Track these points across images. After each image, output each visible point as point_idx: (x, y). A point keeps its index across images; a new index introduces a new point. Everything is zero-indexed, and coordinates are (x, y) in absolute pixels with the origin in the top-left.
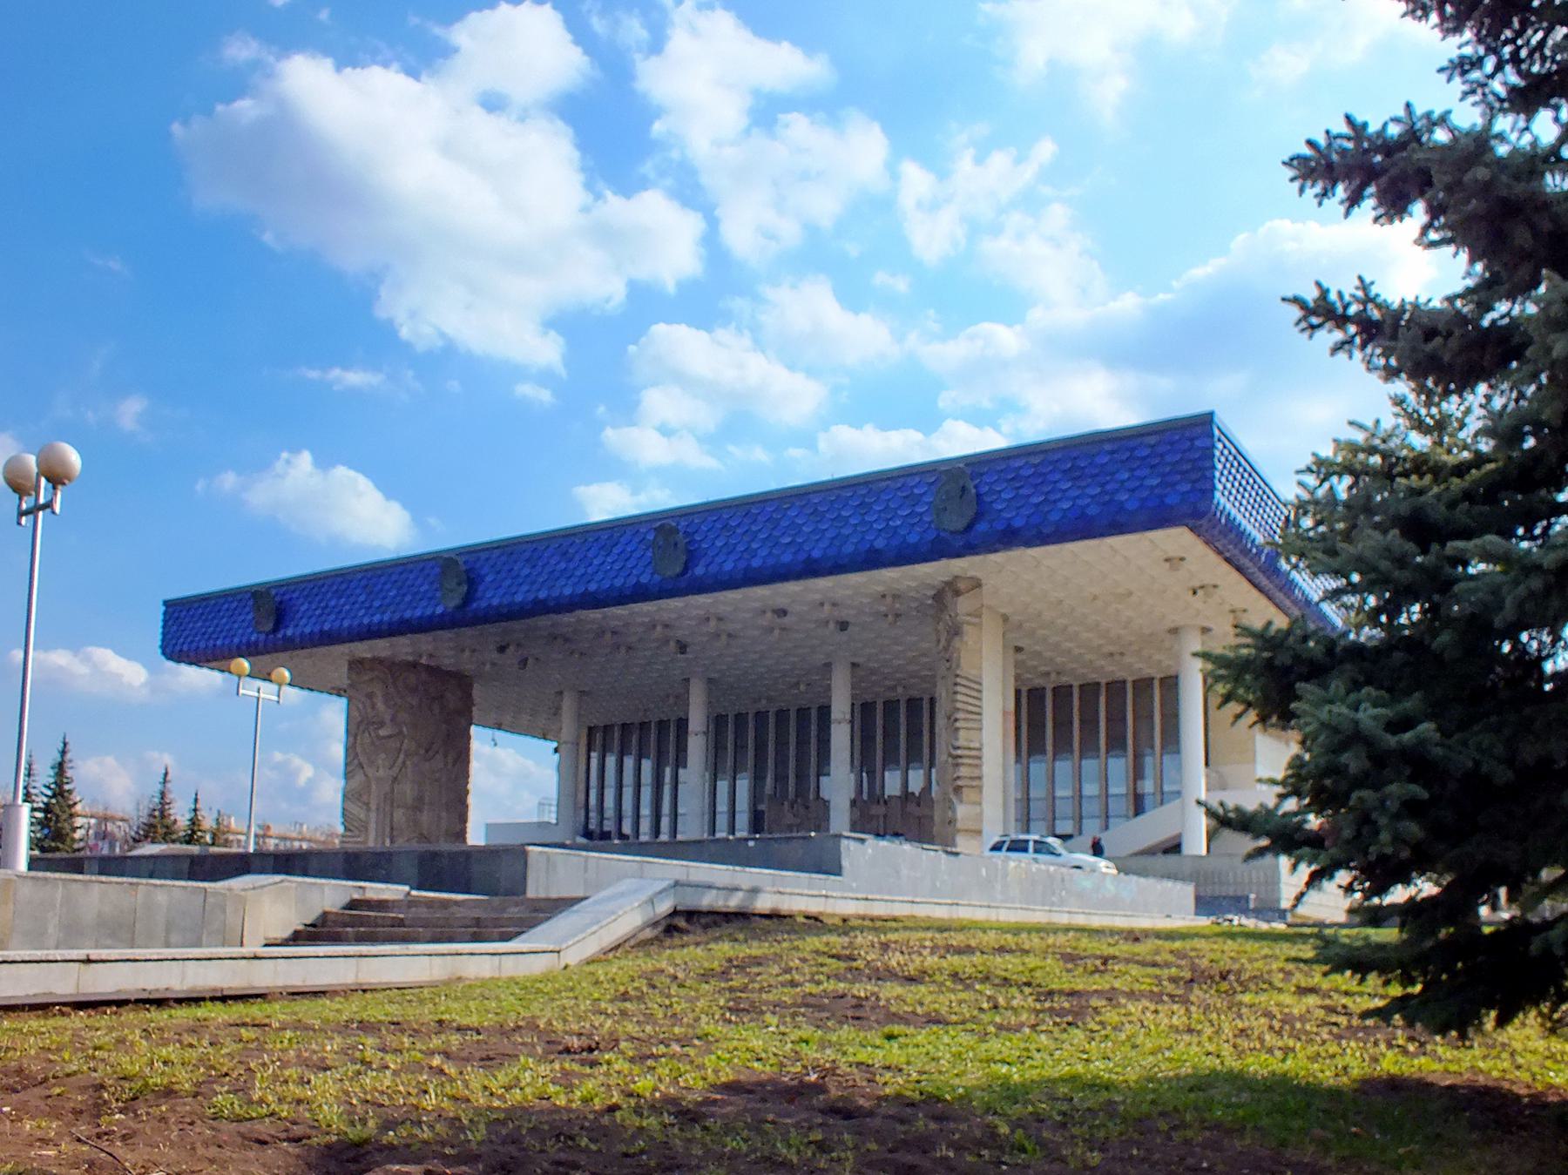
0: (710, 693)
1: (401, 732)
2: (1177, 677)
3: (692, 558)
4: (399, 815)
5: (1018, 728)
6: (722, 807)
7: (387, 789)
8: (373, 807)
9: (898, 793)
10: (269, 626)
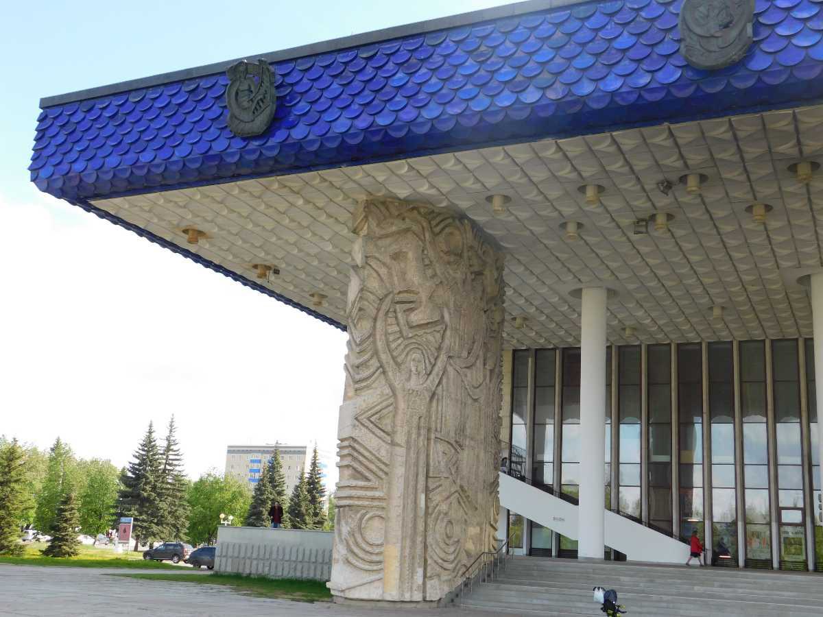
3: (280, 117)
4: (438, 451)
5: (608, 385)
6: (362, 450)
7: (423, 410)
8: (400, 438)
10: (260, 122)
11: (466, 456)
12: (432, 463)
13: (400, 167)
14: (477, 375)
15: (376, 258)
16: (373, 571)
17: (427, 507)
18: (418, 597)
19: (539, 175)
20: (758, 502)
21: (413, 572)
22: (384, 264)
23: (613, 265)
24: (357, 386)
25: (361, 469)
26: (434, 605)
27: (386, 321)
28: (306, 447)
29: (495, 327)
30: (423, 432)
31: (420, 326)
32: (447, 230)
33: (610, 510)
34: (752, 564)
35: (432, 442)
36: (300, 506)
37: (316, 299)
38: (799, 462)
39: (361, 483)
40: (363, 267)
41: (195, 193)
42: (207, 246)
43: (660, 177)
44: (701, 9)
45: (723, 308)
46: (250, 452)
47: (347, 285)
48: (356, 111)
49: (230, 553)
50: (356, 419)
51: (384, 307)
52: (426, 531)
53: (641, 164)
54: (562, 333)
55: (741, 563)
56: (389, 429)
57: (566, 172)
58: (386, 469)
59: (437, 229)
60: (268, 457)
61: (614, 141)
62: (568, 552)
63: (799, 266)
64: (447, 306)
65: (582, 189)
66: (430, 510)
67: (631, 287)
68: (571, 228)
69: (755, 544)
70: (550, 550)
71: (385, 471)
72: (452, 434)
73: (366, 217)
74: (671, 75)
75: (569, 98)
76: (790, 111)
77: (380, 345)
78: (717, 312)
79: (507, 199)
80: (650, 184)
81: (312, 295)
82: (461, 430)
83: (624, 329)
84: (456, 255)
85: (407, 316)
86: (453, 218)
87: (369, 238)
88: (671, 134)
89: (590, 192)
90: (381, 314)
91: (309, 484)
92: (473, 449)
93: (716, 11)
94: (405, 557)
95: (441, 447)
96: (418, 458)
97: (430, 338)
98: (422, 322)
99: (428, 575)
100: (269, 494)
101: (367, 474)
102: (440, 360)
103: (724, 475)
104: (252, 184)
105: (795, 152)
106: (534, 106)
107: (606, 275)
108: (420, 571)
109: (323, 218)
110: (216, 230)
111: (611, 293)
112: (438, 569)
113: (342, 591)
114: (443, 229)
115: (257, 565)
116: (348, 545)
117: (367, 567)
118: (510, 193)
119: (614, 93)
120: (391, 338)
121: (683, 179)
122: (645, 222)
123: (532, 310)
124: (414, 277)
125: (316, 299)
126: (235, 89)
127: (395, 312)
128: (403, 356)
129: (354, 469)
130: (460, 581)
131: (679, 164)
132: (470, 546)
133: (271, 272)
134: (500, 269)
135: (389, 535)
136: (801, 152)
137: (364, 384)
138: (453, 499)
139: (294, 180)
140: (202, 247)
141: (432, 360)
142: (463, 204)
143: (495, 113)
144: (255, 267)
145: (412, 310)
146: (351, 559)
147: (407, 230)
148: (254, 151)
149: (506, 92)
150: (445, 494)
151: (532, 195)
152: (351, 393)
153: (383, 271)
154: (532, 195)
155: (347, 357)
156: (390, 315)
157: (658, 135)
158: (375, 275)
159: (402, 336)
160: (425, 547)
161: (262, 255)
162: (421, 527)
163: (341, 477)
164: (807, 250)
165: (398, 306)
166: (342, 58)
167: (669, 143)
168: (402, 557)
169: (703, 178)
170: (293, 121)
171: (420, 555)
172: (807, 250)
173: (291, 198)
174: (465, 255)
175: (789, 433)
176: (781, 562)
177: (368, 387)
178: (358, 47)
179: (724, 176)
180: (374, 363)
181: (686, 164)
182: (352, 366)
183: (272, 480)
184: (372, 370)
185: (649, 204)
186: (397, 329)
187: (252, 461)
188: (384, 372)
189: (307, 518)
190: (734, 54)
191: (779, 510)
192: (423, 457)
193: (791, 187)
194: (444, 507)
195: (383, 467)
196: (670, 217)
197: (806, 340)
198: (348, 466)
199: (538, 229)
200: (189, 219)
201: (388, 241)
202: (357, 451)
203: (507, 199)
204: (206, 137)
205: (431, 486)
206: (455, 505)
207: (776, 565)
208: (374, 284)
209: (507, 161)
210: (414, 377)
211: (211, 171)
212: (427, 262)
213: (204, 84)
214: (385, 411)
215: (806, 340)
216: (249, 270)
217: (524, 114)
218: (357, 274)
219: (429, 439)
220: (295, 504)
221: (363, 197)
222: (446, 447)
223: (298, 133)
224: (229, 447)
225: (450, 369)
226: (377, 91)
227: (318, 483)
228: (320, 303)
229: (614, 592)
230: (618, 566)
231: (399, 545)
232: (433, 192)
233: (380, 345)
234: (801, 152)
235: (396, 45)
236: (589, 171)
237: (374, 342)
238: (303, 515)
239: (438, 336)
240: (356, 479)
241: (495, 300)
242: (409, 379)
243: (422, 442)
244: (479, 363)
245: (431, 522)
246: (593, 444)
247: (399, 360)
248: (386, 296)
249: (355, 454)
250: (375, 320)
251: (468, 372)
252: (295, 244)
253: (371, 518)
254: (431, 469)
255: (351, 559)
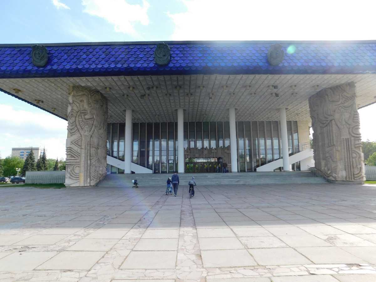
0: (184, 114)
1: (93, 118)
2: (229, 122)
3: (49, 62)
4: (93, 151)
6: (73, 150)
8: (83, 147)
9: (194, 147)
10: (43, 63)
11: (99, 151)
12: (91, 153)
13: (84, 79)
14: (101, 131)
15: (76, 101)
16: (77, 180)
17: (90, 164)
18: (88, 185)
19: (119, 83)
20: (164, 159)
21: (87, 179)
22: (78, 103)
23: (134, 105)
24: (71, 134)
25: (73, 155)
26: (92, 187)
27: (79, 118)
28: (38, 148)
29: (106, 119)
30: (89, 145)
31: (88, 119)
32: (95, 95)
33: (133, 162)
34: (163, 172)
35: (91, 147)
36: (40, 164)
37: (53, 109)
38: (173, 150)
39: (73, 158)
40: (72, 104)
41: (20, 80)
42: (21, 94)
43: (148, 86)
44: (159, 51)
45: (158, 115)
46: (20, 150)
47: (67, 109)
48: (71, 63)
49: (30, 178)
50: (71, 142)
51: (78, 114)
52: (90, 169)
53: (143, 83)
54: (120, 120)
55: (160, 172)
56: (80, 145)
57: (126, 84)
58: (80, 155)
59: (92, 94)
60: (30, 151)
61: (138, 78)
62: (122, 172)
63: (175, 107)
64: (94, 114)
65: (129, 88)
66: (91, 164)
67: (138, 110)
68: (126, 96)
69: (163, 168)
70: (116, 172)
71: (79, 155)
72: (96, 146)
73: (73, 90)
74: (152, 65)
75: (128, 67)
76: (176, 76)
77: (77, 124)
78: (157, 116)
79: (110, 88)
80: (145, 87)
81: (52, 108)
82: (98, 145)
83: (135, 119)
84: (97, 101)
85: (84, 116)
86: (96, 92)
87: (74, 96)
88: (151, 78)
89: (131, 89)
90: (77, 116)
91: (42, 158)
92: (101, 149)
93: (162, 52)
94: (324, 159)
95: (94, 149)
96: (88, 152)
97: (90, 122)
98: (88, 118)
99: (91, 179)
100: (30, 161)
101: (74, 156)
102: (93, 128)
103: (157, 153)
104: (39, 79)
105: (177, 84)
106: (120, 68)
107: (132, 107)
108: (89, 179)
109: (59, 89)
110: (25, 90)
111: (133, 111)
112: (94, 178)
113: (69, 185)
114: (94, 94)
115: (39, 181)
116: (70, 174)
117: (75, 179)
118: (111, 87)
119: (139, 67)
120: (80, 122)
121: (153, 87)
122: (143, 96)
123: (113, 114)
124: (86, 106)
125: (53, 109)
126: (34, 53)
127: (81, 115)
128: (84, 126)
129: (71, 155)
130: (98, 180)
131: (152, 84)
132: (100, 172)
133: (41, 102)
134: (107, 105)
135: (81, 171)
136: (178, 84)
137: (73, 134)
138: (97, 161)
139: (52, 79)
140: (20, 94)
141: (91, 127)
142: (99, 89)
143: (110, 69)
144: (36, 100)
145: (85, 115)
146: (71, 177)
147: (84, 94)
148: (41, 71)
149: (113, 64)
150: (95, 160)
151: (117, 88)
152: (70, 136)
153: (78, 105)
154: (117, 88)
155: (68, 127)
156: (80, 116)
157: (148, 78)
158: (76, 106)
159: (83, 121)
160: (90, 173)
161: (17, 86)
162: (89, 168)
163: (67, 157)
164: (177, 101)
165: (82, 114)
166: (67, 48)
167: (150, 80)
168: (84, 175)
169: (157, 87)
170: (53, 64)
171: (88, 175)
172: (177, 101)
173: (50, 84)
174: (99, 101)
175: (171, 143)
176: (161, 172)
177: (74, 134)
178: (72, 46)
179: (162, 87)
180: (76, 128)
181: (154, 84)
182: (70, 129)
183: (31, 158)
184: (75, 130)
185: (144, 92)
186: (82, 120)
187: (21, 152)
188: (78, 131)
189: (42, 168)
190: (166, 62)
191: (169, 160)
192: (89, 152)
193: (176, 91)
194: (94, 163)
195: (79, 154)
196: (149, 95)
197: (175, 123)
198: (69, 154)
199: (117, 96)
200: (16, 86)
201: (79, 97)
202: (72, 151)
203: (110, 88)
204: (25, 65)
205: (91, 158)
206: (97, 163)
207: (167, 172)
208: (75, 108)
209: (112, 80)
210: (86, 132)
211: (25, 74)
212: (89, 103)
213: (23, 49)
214: (79, 141)
215: (175, 123)
216: (33, 101)
217: (117, 70)
218: (71, 105)
219: (90, 147)
220: (39, 164)
221: (72, 85)
222: (95, 149)
223: (55, 67)
224: (12, 148)
225: (96, 130)
226: (78, 59)
227: (45, 158)
228: (54, 111)
229: (136, 180)
230: (133, 175)
231: (83, 173)
232: (91, 85)
233: (77, 124)
234: (178, 84)
235: (83, 47)
236: (131, 84)
237: (76, 123)
238: (41, 167)
239: (92, 122)
240: (72, 157)
241: (106, 112)
242: (85, 132)
243: (88, 148)
244: (102, 129)
245: (91, 167)
246: (127, 146)
247: (82, 128)
248: (79, 111)
249: (71, 151)
250: (76, 117)
251: (100, 130)
252: (49, 95)
253: (76, 167)
254: (91, 154)
255: (71, 177)
